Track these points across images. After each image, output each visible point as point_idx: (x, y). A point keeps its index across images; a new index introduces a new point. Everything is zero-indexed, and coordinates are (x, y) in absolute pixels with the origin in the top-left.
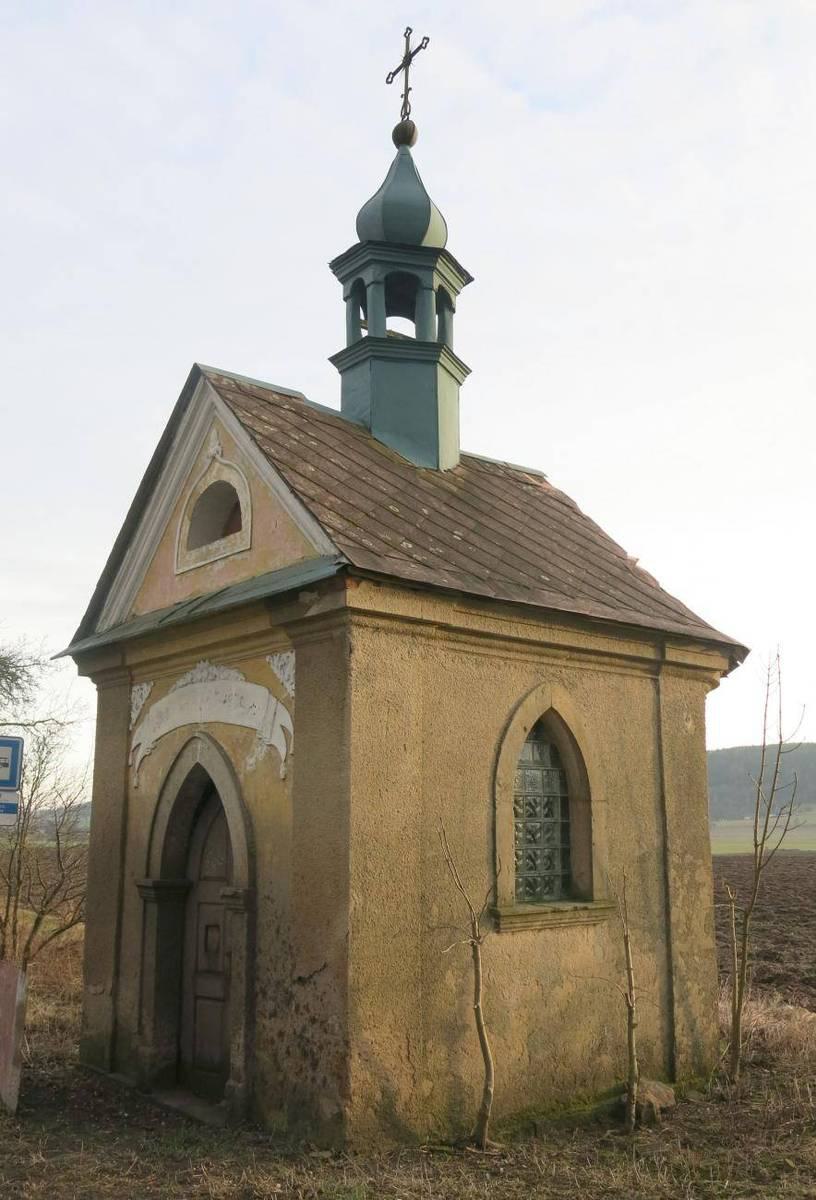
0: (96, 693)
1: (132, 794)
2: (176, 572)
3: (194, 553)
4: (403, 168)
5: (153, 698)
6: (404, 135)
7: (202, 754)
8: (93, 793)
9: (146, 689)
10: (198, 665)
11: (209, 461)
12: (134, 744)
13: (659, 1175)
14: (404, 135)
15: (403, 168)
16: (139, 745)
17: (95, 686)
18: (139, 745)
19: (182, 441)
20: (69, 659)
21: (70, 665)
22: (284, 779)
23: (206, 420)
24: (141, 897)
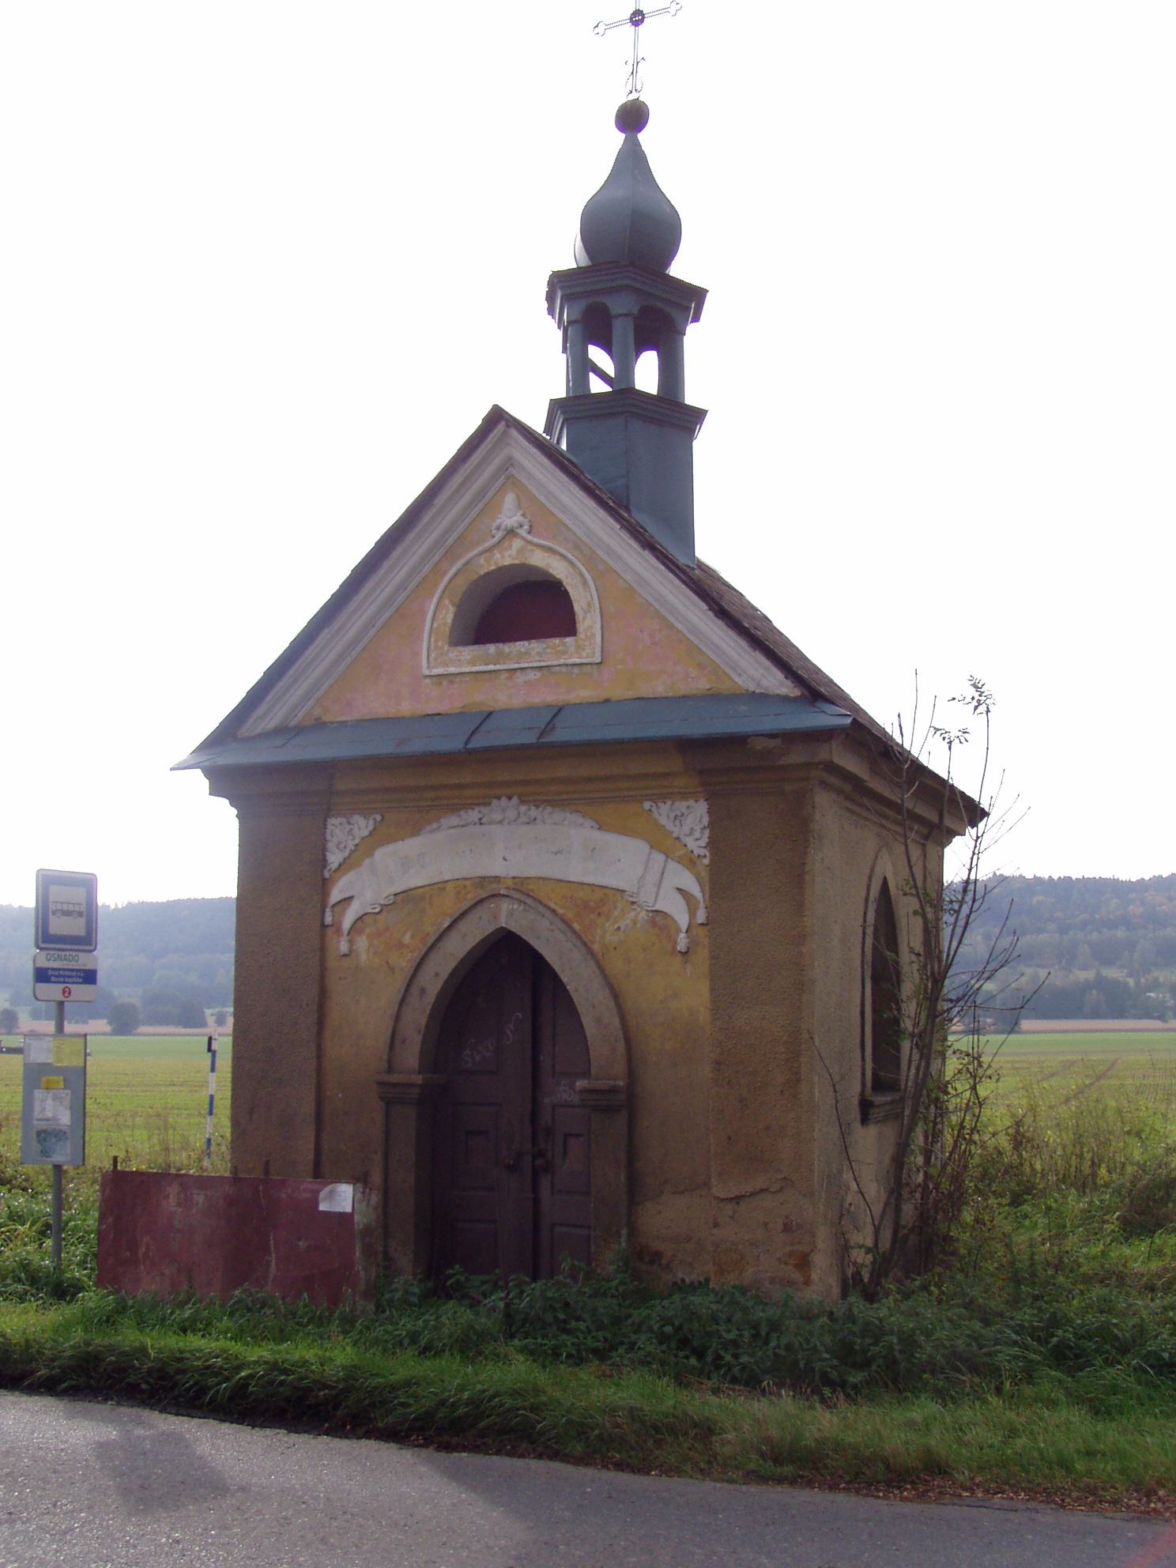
0: (236, 822)
1: (332, 963)
2: (426, 672)
3: (468, 652)
4: (632, 162)
5: (376, 840)
6: (632, 118)
7: (508, 916)
8: (441, 989)
9: (362, 826)
10: (495, 802)
11: (499, 535)
12: (335, 895)
13: (637, 1321)
14: (632, 118)
15: (632, 162)
16: (348, 900)
17: (234, 811)
18: (348, 900)
19: (450, 499)
20: (198, 774)
21: (198, 781)
22: (684, 954)
23: (494, 477)
24: (382, 1098)
